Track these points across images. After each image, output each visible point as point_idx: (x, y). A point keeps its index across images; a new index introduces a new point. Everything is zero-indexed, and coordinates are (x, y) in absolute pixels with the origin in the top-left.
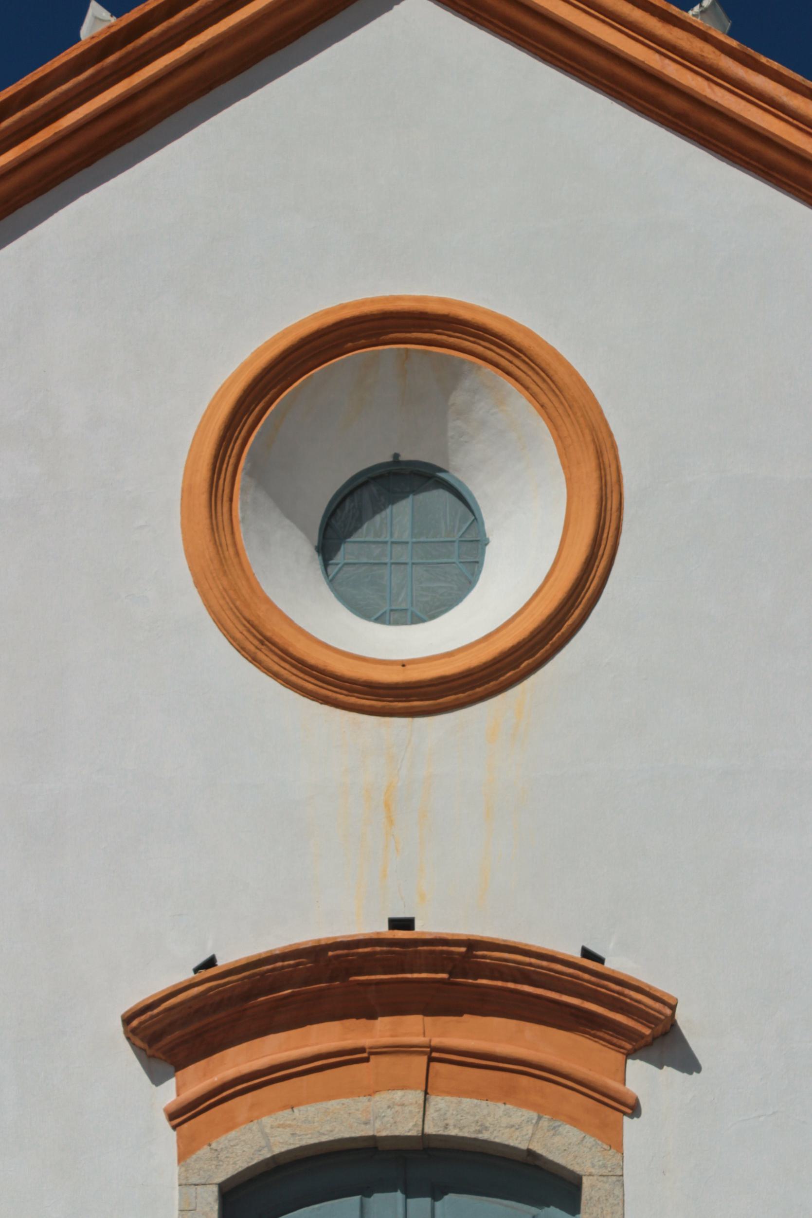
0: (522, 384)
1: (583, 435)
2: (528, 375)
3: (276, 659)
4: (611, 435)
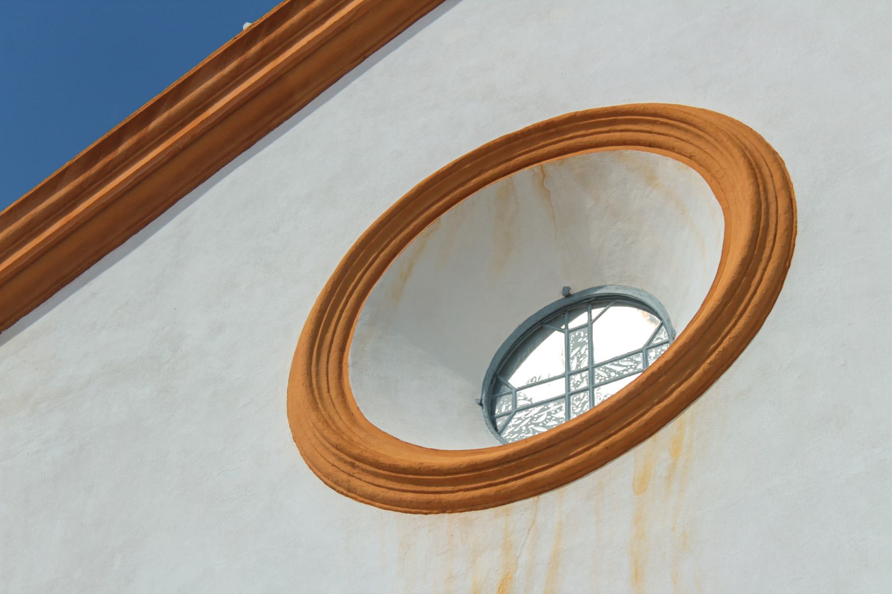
0: (666, 149)
1: (733, 156)
2: (671, 136)
3: (369, 478)
4: (760, 139)
